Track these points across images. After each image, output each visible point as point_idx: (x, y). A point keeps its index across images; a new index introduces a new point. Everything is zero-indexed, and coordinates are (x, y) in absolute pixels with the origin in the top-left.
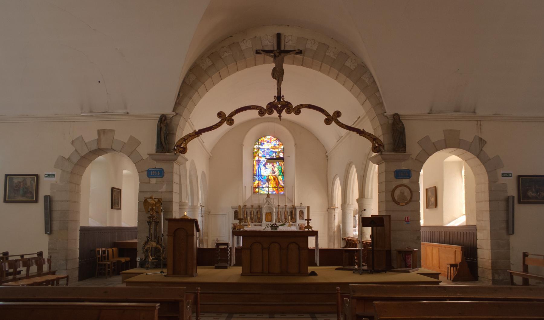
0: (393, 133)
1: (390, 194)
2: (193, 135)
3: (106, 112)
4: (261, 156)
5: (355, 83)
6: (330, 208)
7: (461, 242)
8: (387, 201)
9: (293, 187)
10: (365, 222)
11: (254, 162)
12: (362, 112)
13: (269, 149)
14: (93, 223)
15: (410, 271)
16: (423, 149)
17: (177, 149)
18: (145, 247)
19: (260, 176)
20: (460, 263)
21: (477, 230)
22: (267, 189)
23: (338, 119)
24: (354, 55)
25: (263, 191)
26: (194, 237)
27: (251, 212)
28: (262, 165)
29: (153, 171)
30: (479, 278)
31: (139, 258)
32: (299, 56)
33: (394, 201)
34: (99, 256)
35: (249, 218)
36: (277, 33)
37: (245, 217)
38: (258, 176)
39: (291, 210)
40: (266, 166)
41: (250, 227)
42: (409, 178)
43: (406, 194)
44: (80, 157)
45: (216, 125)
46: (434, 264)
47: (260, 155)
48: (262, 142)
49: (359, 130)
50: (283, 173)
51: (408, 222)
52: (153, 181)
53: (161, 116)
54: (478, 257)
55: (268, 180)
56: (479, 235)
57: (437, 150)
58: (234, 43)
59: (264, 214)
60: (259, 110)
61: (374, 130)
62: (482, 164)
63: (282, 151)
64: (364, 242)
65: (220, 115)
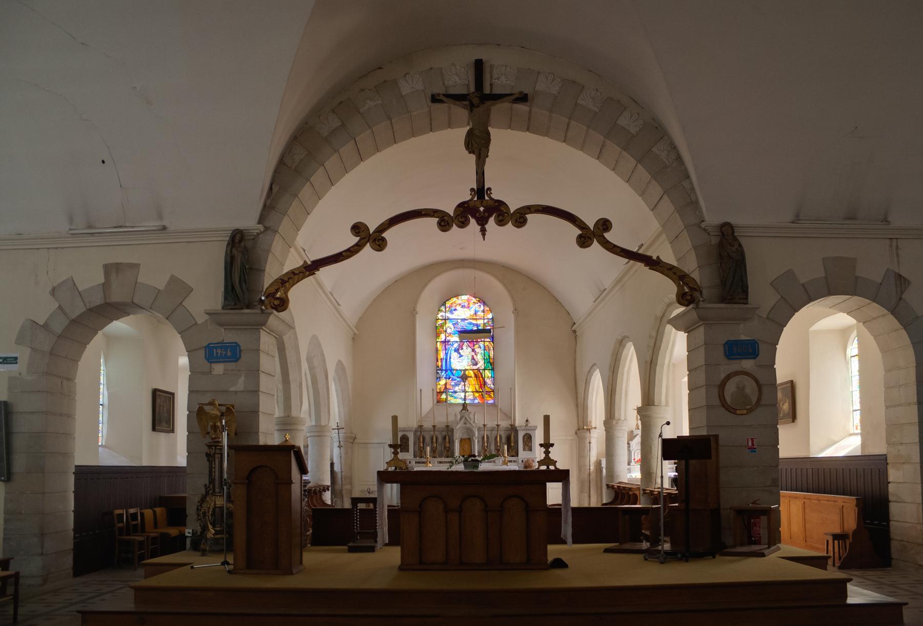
0: (719, 264)
1: (715, 391)
2: (300, 272)
3: (121, 227)
4: (450, 334)
5: (639, 161)
6: (582, 429)
7: (857, 492)
8: (709, 407)
9: (512, 390)
10: (672, 448)
11: (438, 343)
12: (655, 226)
13: (466, 320)
14: (108, 458)
15: (766, 552)
16: (782, 297)
17: (266, 302)
18: (201, 507)
19: (449, 371)
20: (855, 532)
21: (888, 464)
22: (462, 395)
23: (606, 235)
24: (637, 103)
25: (456, 398)
26: (292, 485)
27: (432, 439)
28: (453, 349)
29: (216, 348)
30: (893, 562)
31: (191, 531)
32: (522, 108)
33: (723, 406)
34: (120, 525)
35: (428, 449)
36: (476, 60)
37: (421, 447)
38: (446, 371)
39: (507, 433)
40: (460, 351)
41: (431, 465)
42: (754, 358)
43: (748, 390)
44: (67, 322)
45: (348, 250)
46: (792, 533)
47: (449, 331)
48: (452, 307)
49: (650, 258)
50: (492, 364)
51: (752, 449)
52: (219, 369)
53: (232, 234)
54: (891, 518)
55: (464, 378)
56: (893, 475)
57: (810, 299)
58: (385, 81)
59: (457, 441)
60: (438, 219)
61: (678, 260)
62: (902, 327)
63: (490, 323)
64: (654, 491)
65: (358, 229)
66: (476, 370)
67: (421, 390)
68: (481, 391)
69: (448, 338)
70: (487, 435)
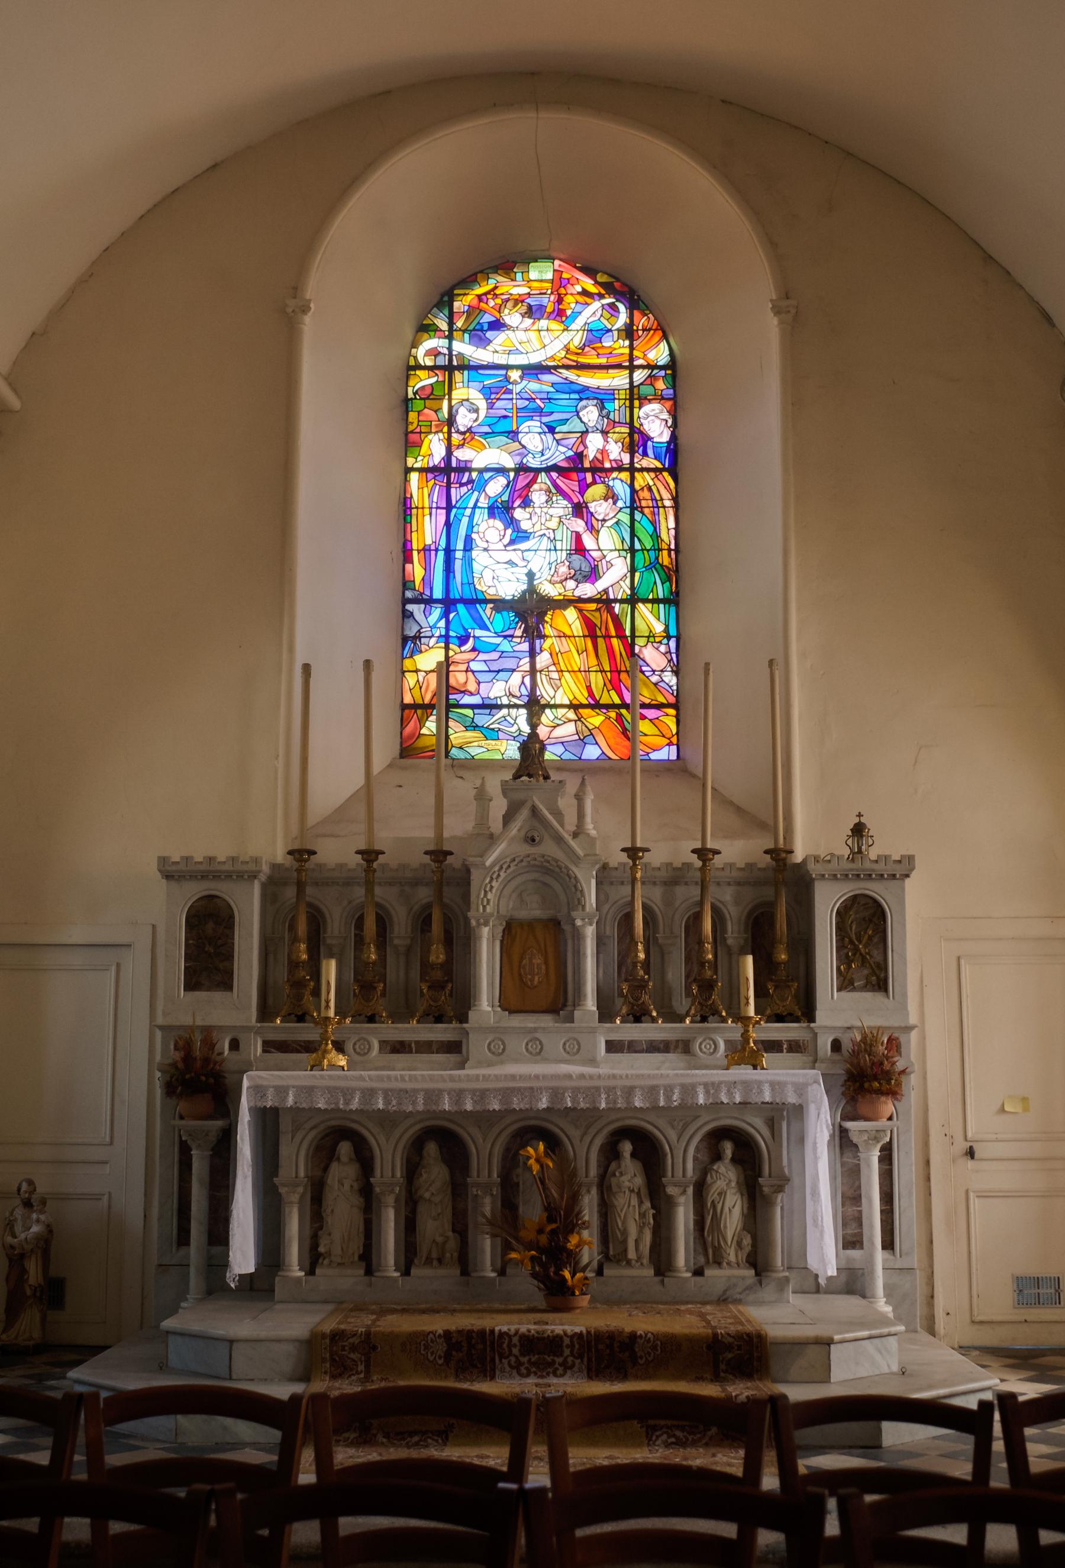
11: (414, 477)
28: (483, 502)
38: (448, 604)
40: (519, 514)
47: (464, 419)
59: (485, 931)
66: (590, 600)
67: (307, 668)
68: (617, 701)
69: (462, 454)
70: (645, 907)
